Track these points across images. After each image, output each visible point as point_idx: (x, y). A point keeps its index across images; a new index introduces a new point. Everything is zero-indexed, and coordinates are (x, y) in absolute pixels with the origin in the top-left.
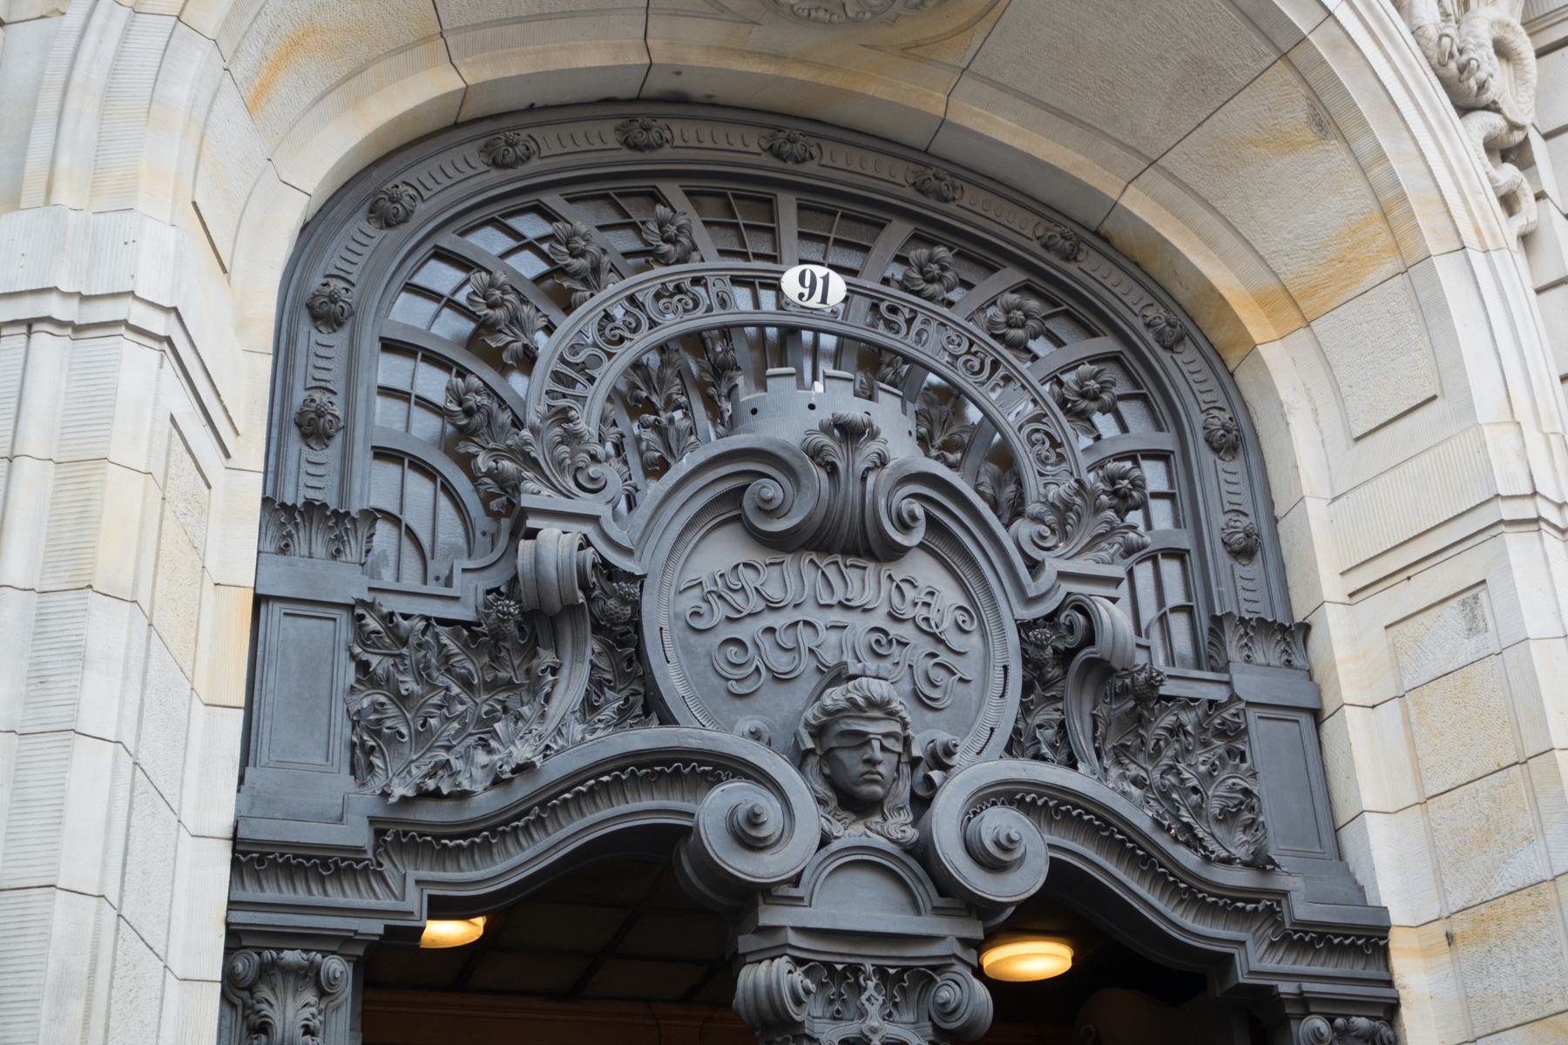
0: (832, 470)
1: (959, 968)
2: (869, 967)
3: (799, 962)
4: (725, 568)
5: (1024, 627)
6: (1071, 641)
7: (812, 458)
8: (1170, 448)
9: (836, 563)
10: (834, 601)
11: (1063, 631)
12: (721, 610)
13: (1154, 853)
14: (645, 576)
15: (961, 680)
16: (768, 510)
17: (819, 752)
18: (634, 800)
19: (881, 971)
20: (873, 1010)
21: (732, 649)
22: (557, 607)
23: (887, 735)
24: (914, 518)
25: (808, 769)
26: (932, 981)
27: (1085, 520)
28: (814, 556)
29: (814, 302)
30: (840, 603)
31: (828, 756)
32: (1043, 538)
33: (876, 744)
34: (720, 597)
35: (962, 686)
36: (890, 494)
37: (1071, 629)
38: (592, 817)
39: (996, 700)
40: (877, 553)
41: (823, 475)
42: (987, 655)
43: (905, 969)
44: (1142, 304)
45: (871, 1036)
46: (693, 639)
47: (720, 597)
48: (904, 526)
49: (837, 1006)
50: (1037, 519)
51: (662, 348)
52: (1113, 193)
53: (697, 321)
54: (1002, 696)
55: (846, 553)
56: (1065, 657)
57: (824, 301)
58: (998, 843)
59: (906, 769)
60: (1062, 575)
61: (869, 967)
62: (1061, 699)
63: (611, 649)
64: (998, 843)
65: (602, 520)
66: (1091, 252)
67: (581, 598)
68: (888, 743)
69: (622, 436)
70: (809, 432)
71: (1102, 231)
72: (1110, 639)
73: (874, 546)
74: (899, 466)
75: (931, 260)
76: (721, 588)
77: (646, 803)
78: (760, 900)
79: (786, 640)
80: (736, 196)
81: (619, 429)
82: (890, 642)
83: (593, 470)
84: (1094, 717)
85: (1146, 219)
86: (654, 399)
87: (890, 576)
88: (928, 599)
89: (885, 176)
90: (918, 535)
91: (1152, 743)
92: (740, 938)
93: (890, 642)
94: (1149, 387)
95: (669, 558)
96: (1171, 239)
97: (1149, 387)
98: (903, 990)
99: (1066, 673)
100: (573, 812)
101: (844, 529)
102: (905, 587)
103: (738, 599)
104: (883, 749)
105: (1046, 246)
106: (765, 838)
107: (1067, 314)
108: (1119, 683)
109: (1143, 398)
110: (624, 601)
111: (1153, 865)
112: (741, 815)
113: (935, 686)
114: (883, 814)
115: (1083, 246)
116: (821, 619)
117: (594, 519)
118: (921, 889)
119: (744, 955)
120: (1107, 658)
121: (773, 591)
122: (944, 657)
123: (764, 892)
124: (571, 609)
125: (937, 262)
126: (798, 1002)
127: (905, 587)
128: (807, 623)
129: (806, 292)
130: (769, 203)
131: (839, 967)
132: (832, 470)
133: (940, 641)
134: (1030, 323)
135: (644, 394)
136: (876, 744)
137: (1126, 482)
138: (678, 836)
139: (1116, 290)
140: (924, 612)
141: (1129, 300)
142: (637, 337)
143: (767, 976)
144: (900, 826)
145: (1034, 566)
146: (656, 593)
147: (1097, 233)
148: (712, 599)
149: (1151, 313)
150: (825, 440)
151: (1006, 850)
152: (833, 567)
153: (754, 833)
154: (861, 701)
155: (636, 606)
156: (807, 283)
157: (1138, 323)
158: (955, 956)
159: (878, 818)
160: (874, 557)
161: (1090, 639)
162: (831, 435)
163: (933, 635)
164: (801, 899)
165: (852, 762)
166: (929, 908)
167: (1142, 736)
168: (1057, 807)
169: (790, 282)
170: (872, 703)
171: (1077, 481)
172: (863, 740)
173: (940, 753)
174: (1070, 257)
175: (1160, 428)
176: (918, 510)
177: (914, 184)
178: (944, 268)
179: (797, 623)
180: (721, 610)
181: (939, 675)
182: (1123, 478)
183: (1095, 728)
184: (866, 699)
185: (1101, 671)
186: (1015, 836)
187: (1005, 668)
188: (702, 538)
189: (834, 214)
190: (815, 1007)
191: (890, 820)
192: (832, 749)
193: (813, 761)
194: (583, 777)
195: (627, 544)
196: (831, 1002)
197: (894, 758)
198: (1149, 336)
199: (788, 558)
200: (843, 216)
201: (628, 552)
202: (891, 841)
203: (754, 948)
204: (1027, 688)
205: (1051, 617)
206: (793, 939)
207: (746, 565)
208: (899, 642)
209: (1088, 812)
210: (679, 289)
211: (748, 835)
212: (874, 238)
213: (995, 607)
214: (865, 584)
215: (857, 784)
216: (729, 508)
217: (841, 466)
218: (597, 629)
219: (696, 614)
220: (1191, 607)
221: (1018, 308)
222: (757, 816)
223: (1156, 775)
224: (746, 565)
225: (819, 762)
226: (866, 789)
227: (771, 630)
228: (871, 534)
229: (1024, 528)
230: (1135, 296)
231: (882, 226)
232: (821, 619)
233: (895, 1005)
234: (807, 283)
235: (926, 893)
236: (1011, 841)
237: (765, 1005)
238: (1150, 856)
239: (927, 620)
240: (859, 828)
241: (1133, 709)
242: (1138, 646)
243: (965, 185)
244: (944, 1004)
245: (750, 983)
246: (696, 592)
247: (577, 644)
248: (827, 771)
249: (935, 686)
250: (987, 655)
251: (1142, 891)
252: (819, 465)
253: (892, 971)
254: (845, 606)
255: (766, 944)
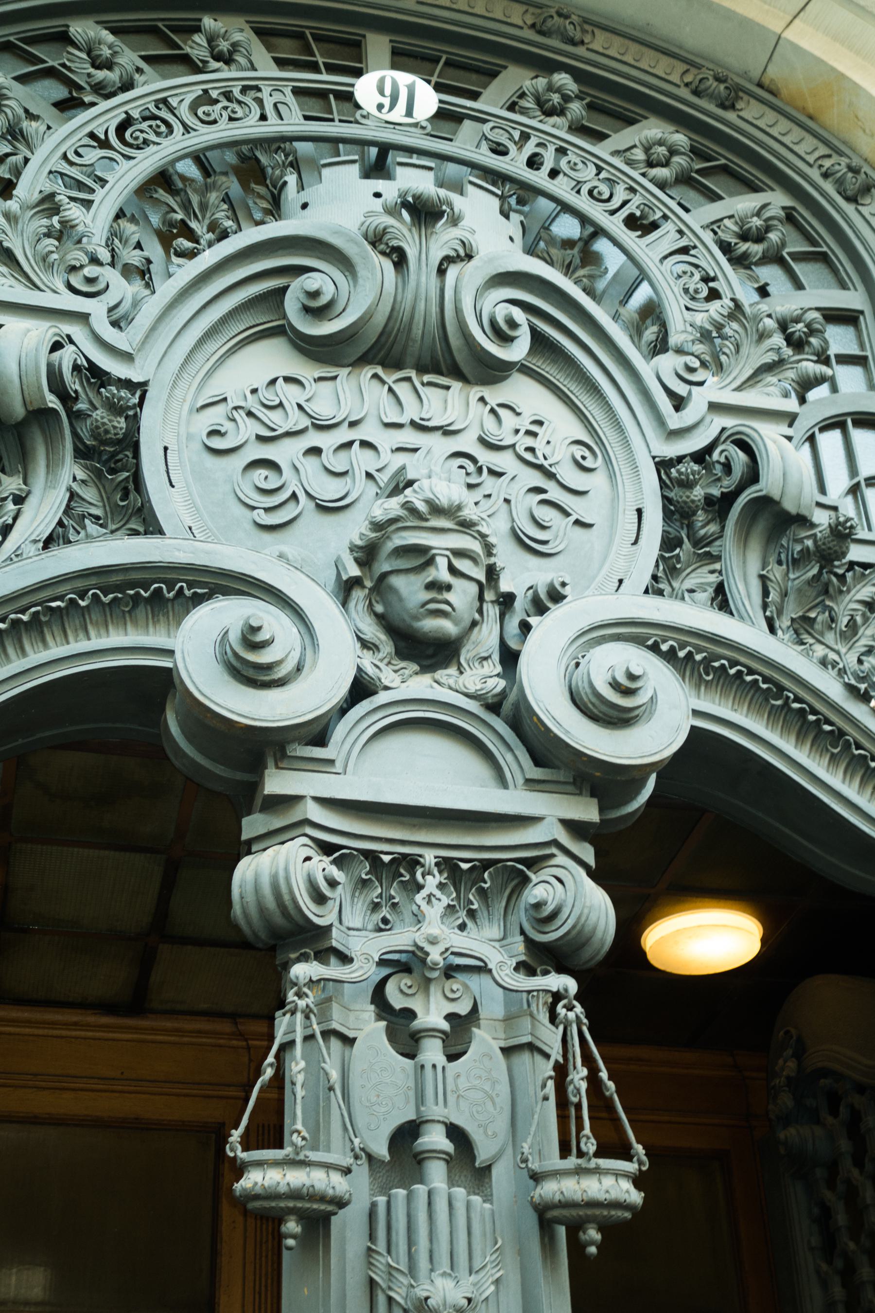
0: (399, 258)
1: (561, 859)
2: (429, 857)
3: (327, 849)
4: (260, 382)
5: (663, 465)
6: (728, 484)
7: (373, 244)
8: (858, 306)
9: (408, 379)
10: (404, 419)
11: (718, 470)
12: (249, 429)
13: (847, 728)
14: (145, 384)
15: (577, 522)
16: (318, 311)
17: (368, 584)
18: (99, 636)
19: (447, 865)
20: (434, 912)
21: (261, 473)
22: (19, 412)
23: (460, 553)
24: (512, 324)
25: (352, 605)
26: (526, 880)
27: (744, 350)
28: (379, 370)
29: (398, 115)
30: (413, 423)
31: (381, 587)
32: (691, 370)
33: (442, 563)
34: (250, 414)
35: (578, 530)
36: (479, 294)
37: (727, 467)
38: (36, 656)
39: (627, 548)
40: (466, 369)
41: (388, 265)
42: (615, 498)
43: (487, 864)
44: (817, 154)
45: (428, 948)
46: (211, 461)
47: (250, 414)
48: (503, 337)
49: (385, 912)
50: (679, 351)
51: (199, 158)
52: (775, 25)
53: (250, 127)
54: (635, 543)
55: (422, 370)
56: (719, 506)
57: (409, 113)
58: (615, 685)
59: (492, 611)
60: (714, 407)
61: (429, 857)
62: (718, 558)
63: (99, 474)
64: (615, 685)
65: (92, 319)
66: (753, 101)
67: (52, 401)
68: (463, 565)
69: (149, 261)
70: (368, 214)
71: (766, 82)
72: (779, 474)
73: (461, 357)
74: (491, 260)
75: (550, 88)
76: (252, 403)
77: (116, 638)
78: (270, 763)
79: (338, 463)
80: (317, 38)
81: (146, 253)
82: (480, 470)
83: (90, 271)
84: (763, 578)
85: (817, 53)
86: (194, 225)
87: (482, 399)
88: (534, 428)
89: (499, 15)
90: (518, 350)
91: (845, 620)
92: (245, 821)
93: (480, 470)
94: (830, 244)
95: (183, 366)
96: (849, 73)
97: (830, 244)
98: (483, 894)
99: (723, 528)
100: (11, 650)
101: (417, 331)
102: (501, 412)
103: (275, 417)
104: (452, 570)
105: (696, 93)
106: (269, 667)
107: (725, 170)
108: (798, 548)
109: (823, 258)
110: (116, 408)
111: (847, 745)
112: (234, 637)
113: (543, 527)
114: (460, 665)
115: (741, 94)
116: (386, 440)
117: (83, 318)
118: (509, 757)
119: (250, 842)
120: (776, 496)
121: (323, 409)
122: (555, 493)
123: (266, 746)
124: (41, 416)
125: (558, 90)
126: (320, 899)
127: (501, 412)
128: (365, 444)
129: (387, 102)
130: (355, 48)
131: (386, 858)
132: (399, 258)
133: (550, 475)
134: (676, 159)
135: (179, 216)
136: (442, 563)
137: (800, 326)
138: (156, 685)
139: (784, 139)
140: (529, 442)
141: (800, 149)
142: (165, 142)
143: (272, 869)
144: (480, 676)
145: (679, 403)
146: (161, 405)
147: (760, 85)
148: (240, 416)
149: (827, 163)
150: (390, 221)
151: (628, 692)
152: (405, 385)
153: (252, 657)
154: (422, 507)
155: (134, 421)
156: (388, 91)
157: (815, 174)
158: (555, 843)
159: (452, 671)
160: (457, 373)
161: (753, 476)
162: (398, 216)
163: (539, 468)
164: (331, 762)
165: (410, 590)
166: (520, 781)
167: (831, 609)
168: (707, 661)
169: (366, 89)
170: (436, 509)
171: (732, 300)
172: (422, 557)
173: (543, 595)
174: (728, 105)
175: (843, 286)
176: (518, 315)
177: (533, 26)
178: (566, 99)
179: (350, 444)
180: (249, 429)
181: (546, 514)
182: (797, 320)
183: (766, 593)
184: (428, 502)
185: (776, 521)
186: (636, 671)
187: (639, 512)
188: (232, 351)
189: (437, 61)
190: (356, 914)
191: (468, 672)
192: (384, 576)
193: (358, 594)
194: (25, 602)
195: (124, 346)
196: (375, 907)
197: (474, 589)
198: (828, 187)
199: (343, 372)
200: (448, 63)
201: (127, 357)
202: (467, 695)
203: (262, 831)
204: (669, 543)
205: (700, 457)
206: (315, 813)
207: (288, 379)
208: (491, 472)
209: (751, 672)
210: (228, 95)
211: (249, 669)
212: (485, 87)
213: (626, 443)
214: (451, 403)
215: (417, 618)
216: (265, 316)
217: (411, 253)
218: (82, 453)
219: (214, 433)
220: (865, 358)
221: (661, 143)
222: (256, 630)
223: (851, 659)
224: (288, 379)
225: (369, 597)
226: (430, 625)
227: (315, 451)
228: (455, 341)
229: (668, 363)
230: (807, 145)
231: (494, 75)
232: (386, 440)
233: (472, 914)
234: (388, 91)
235: (516, 761)
236: (632, 677)
237: (270, 902)
238: (842, 733)
239: (531, 450)
240: (426, 679)
241: (817, 577)
242: (819, 505)
243: (596, 31)
244: (538, 906)
245: (250, 876)
246: (220, 409)
247: (52, 466)
248: (379, 608)
249: (543, 527)
250: (615, 498)
251: (835, 780)
252: (383, 253)
253: (465, 866)
254: (419, 427)
255: (278, 823)
